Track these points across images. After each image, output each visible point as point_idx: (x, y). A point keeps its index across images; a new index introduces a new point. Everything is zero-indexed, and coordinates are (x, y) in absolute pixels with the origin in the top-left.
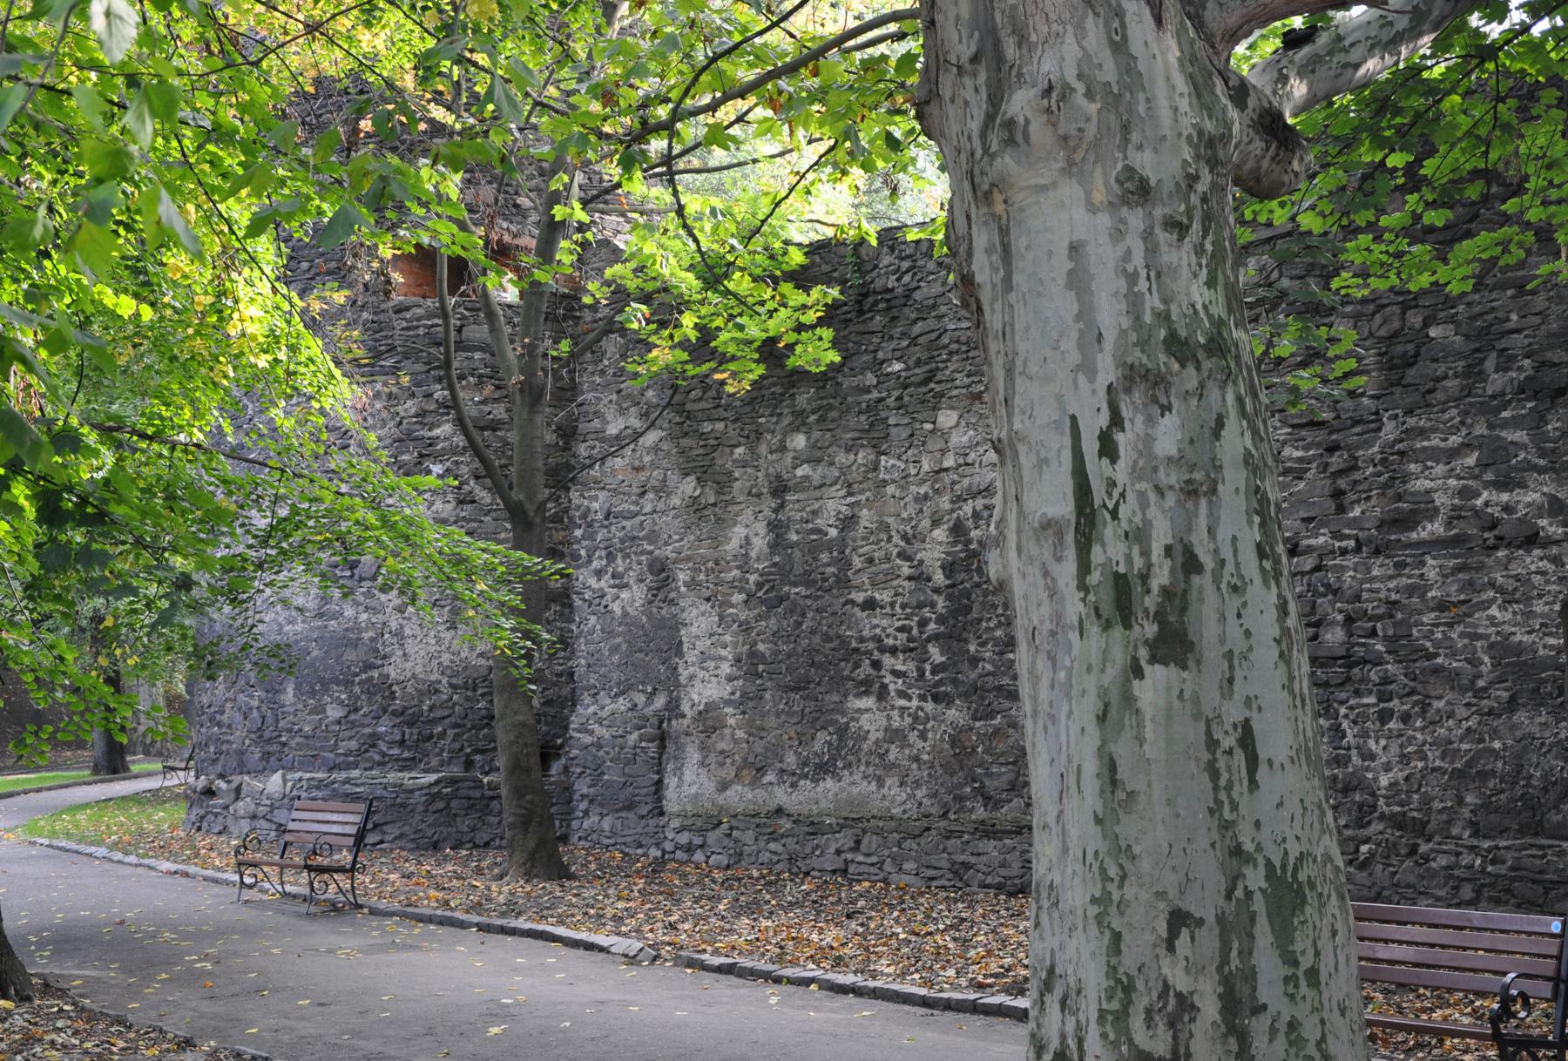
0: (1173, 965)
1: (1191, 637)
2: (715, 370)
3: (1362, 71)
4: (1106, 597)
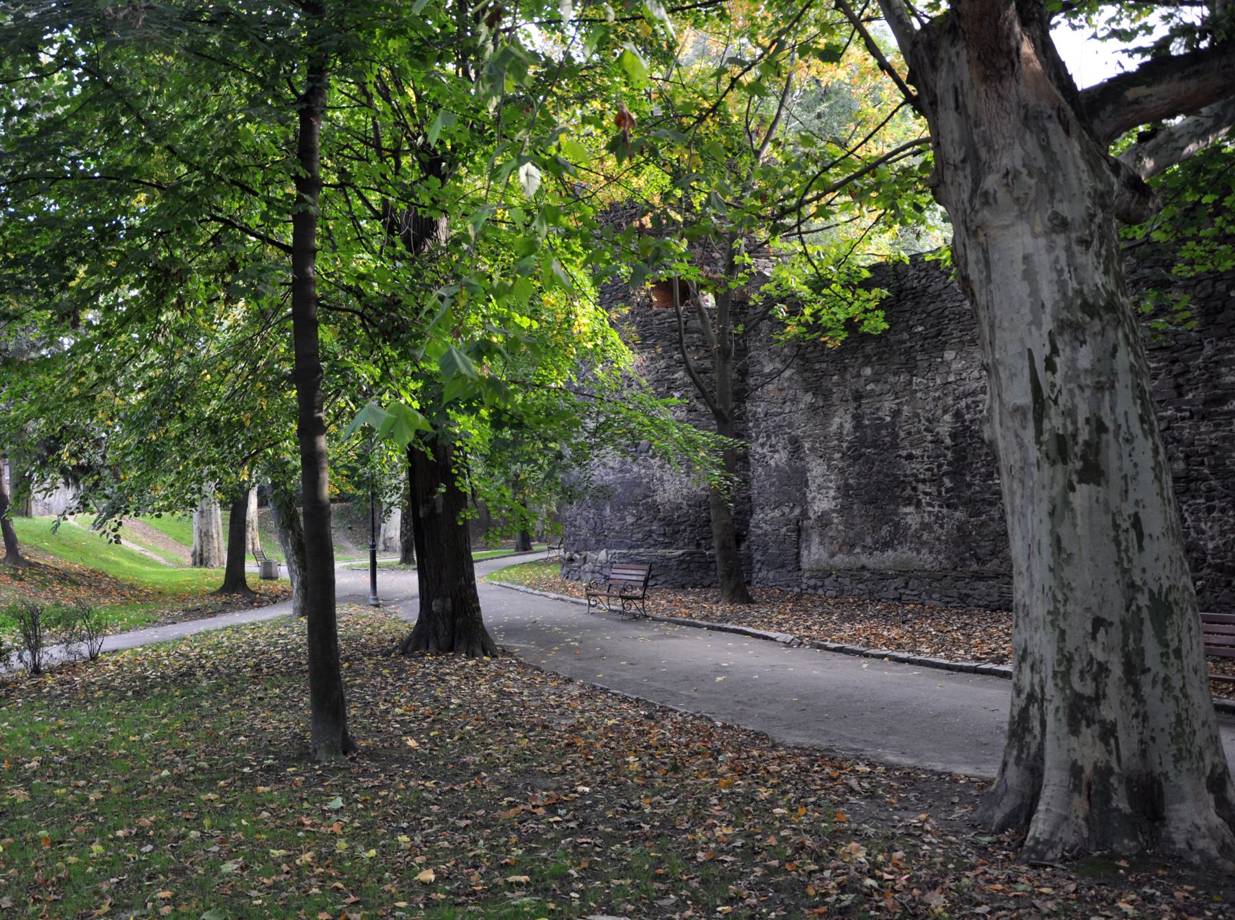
0: (1096, 647)
1: (1103, 467)
2: (821, 336)
3: (1186, 151)
4: (1052, 448)
